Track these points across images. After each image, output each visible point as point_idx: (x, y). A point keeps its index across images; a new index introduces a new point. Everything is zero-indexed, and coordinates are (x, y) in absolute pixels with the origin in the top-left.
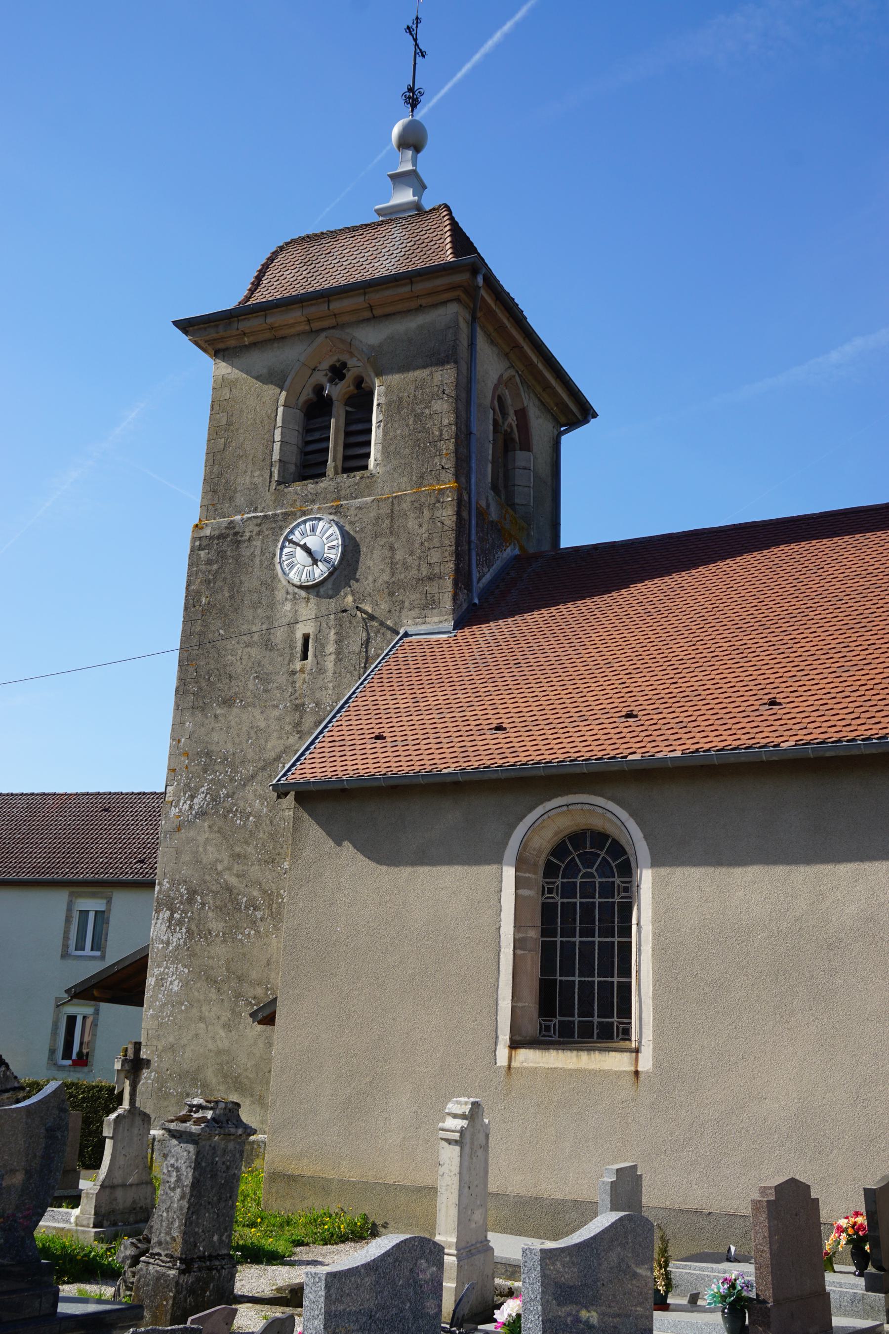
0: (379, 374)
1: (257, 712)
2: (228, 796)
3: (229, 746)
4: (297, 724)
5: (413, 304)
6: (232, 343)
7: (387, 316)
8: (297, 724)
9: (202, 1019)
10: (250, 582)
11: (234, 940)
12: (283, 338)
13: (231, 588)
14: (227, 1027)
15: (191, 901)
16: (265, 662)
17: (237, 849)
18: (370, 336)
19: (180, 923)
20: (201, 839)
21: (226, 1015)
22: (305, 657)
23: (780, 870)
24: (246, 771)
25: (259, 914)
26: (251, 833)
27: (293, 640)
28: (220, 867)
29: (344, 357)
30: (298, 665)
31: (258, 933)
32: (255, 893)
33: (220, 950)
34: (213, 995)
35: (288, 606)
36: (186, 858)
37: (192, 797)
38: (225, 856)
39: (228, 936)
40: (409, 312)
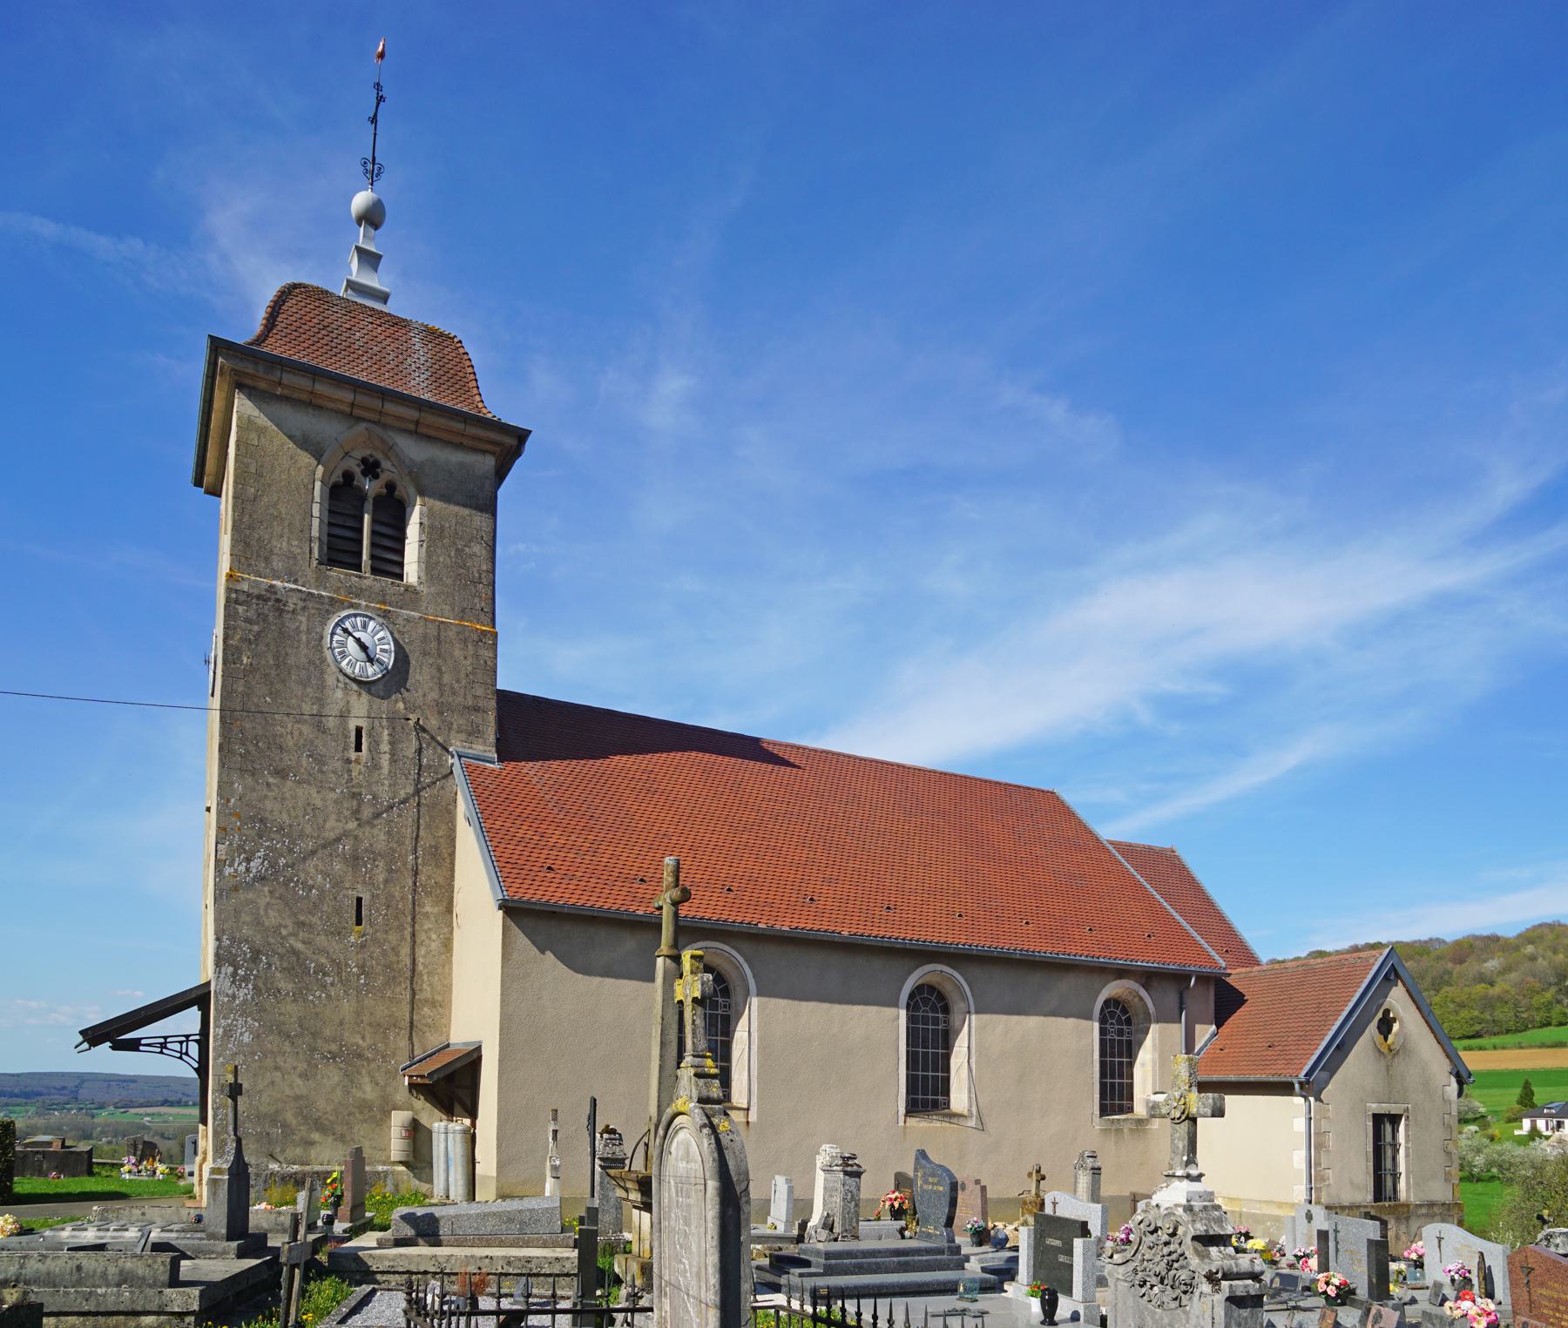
0: (422, 493)
1: (313, 791)
2: (287, 865)
3: (285, 816)
4: (356, 813)
5: (458, 439)
6: (262, 385)
8: (356, 813)
9: (277, 1068)
10: (299, 655)
12: (320, 407)
13: (276, 656)
14: (304, 1076)
15: (255, 958)
16: (318, 742)
17: (302, 918)
18: (414, 450)
19: (245, 979)
20: (262, 902)
21: (302, 1066)
22: (358, 748)
23: (826, 1006)
25: (329, 980)
27: (345, 728)
28: (284, 932)
29: (379, 456)
30: (353, 755)
31: (329, 997)
32: (323, 960)
33: (291, 1010)
34: (287, 1047)
35: (339, 694)
36: (245, 918)
37: (248, 860)
38: (289, 922)
39: (299, 996)
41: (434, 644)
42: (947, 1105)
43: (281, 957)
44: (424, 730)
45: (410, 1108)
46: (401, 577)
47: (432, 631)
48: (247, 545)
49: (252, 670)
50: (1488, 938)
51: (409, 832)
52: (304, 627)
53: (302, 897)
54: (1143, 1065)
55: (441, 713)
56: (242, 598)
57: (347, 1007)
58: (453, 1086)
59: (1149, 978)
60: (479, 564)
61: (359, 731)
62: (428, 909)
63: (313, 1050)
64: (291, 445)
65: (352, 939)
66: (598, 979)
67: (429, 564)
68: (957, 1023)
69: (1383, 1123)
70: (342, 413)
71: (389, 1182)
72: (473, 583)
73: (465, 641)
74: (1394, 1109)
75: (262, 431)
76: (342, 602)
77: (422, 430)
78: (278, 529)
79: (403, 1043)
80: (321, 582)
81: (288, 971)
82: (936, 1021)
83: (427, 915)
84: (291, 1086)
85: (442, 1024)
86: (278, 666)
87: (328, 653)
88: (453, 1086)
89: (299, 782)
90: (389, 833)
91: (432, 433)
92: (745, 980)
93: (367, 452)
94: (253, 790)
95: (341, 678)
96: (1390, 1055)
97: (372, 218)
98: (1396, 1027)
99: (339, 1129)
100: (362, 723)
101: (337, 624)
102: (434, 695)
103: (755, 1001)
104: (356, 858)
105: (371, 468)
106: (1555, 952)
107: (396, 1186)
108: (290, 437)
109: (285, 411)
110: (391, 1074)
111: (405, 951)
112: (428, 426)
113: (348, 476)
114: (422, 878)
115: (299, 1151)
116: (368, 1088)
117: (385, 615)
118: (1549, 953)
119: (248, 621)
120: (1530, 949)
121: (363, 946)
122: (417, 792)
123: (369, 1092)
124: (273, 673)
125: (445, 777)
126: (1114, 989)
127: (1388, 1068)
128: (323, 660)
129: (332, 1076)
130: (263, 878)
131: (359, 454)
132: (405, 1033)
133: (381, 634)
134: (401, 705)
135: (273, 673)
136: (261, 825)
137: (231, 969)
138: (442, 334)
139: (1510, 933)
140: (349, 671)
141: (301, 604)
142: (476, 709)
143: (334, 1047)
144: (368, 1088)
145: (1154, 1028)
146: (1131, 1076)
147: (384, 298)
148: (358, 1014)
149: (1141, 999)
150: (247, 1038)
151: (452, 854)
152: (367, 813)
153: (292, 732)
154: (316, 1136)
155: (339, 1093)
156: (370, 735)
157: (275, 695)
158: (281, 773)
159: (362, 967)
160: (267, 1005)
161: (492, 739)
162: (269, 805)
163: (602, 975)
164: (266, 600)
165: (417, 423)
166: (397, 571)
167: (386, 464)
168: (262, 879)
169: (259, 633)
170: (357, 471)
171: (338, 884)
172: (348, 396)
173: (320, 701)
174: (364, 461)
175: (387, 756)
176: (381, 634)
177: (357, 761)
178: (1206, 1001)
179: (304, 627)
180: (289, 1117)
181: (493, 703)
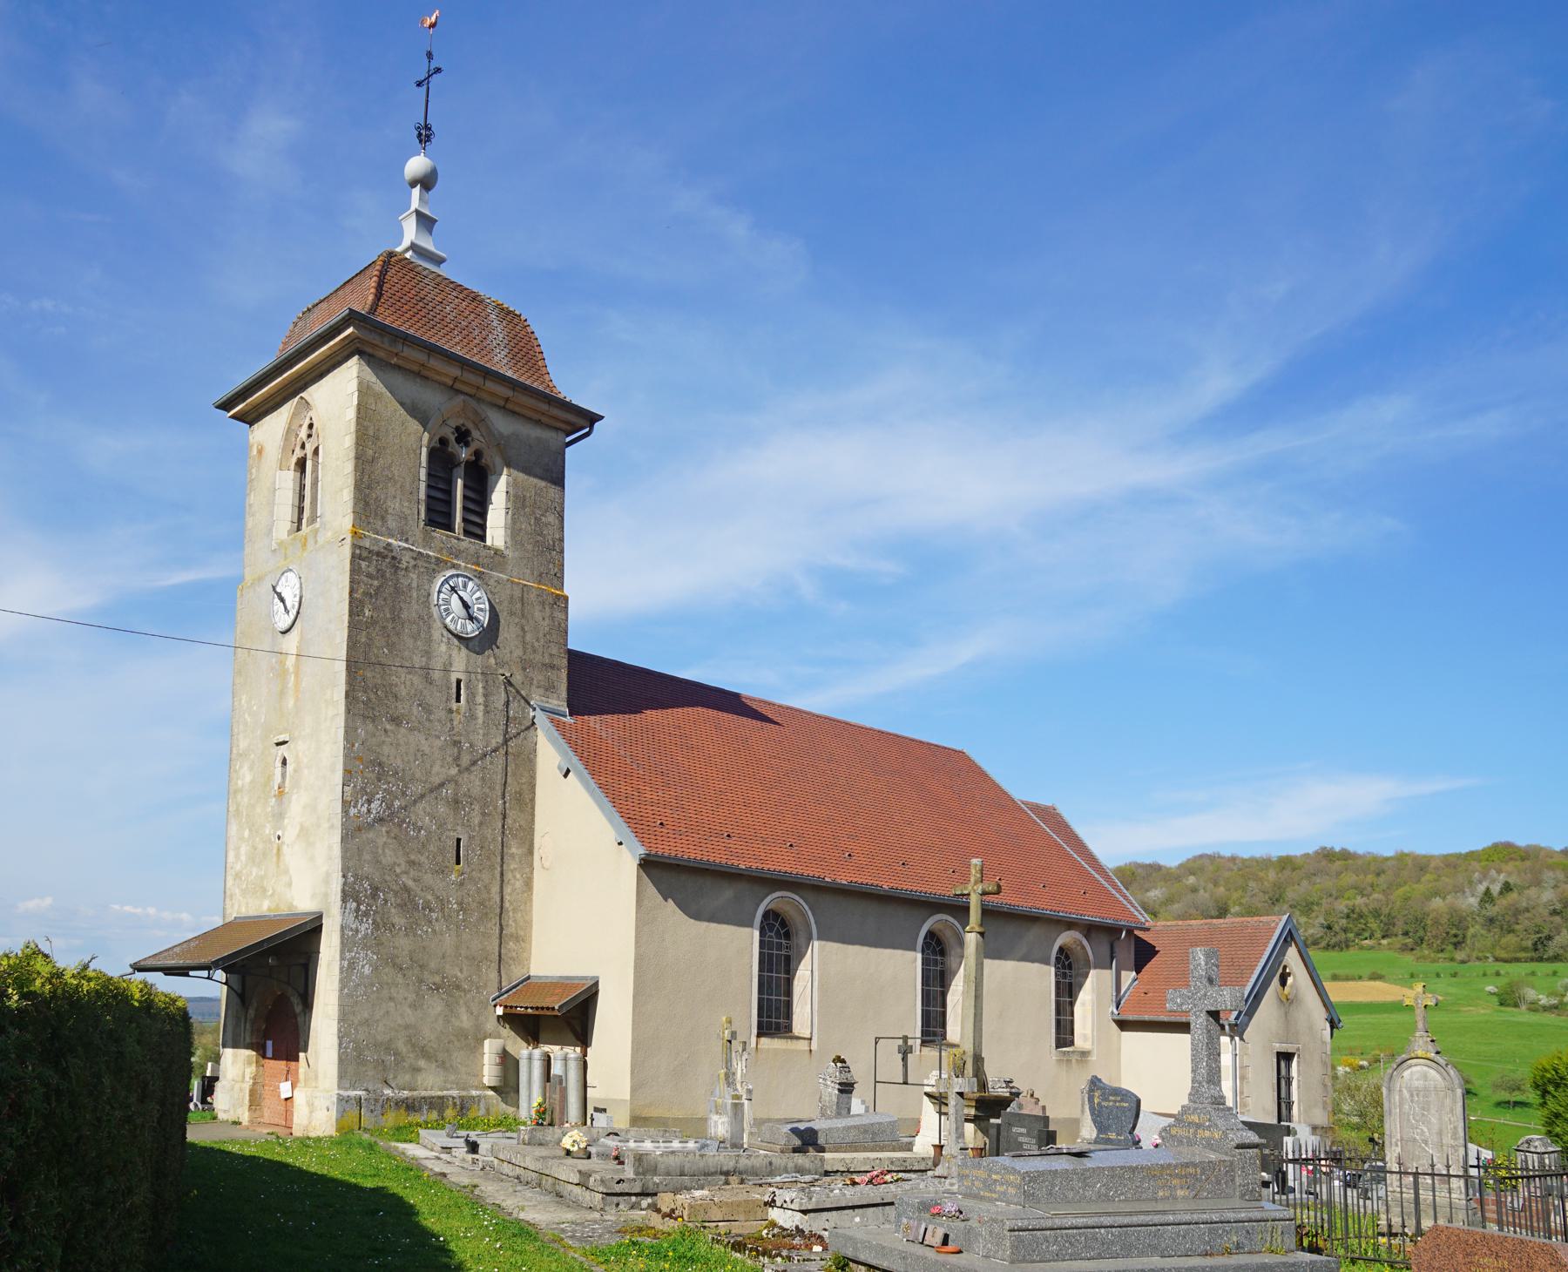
0: (509, 466)
1: (422, 738)
2: (401, 808)
3: (399, 762)
4: (457, 759)
5: (536, 417)
6: (381, 354)
7: (514, 413)
8: (457, 759)
9: (391, 999)
10: (410, 612)
11: (415, 935)
12: (427, 378)
13: (392, 611)
14: (413, 1006)
15: (374, 896)
16: (425, 692)
17: (413, 857)
18: (502, 424)
19: (366, 914)
20: (381, 841)
21: (412, 997)
22: (458, 700)
23: (866, 949)
24: (417, 789)
25: (434, 915)
26: (424, 846)
27: (448, 680)
28: (398, 870)
29: (470, 426)
30: (454, 706)
31: (434, 931)
32: (430, 897)
33: (404, 944)
34: (400, 979)
35: (443, 648)
36: (367, 857)
37: (369, 802)
38: (402, 861)
39: (410, 930)
40: (530, 419)
41: (519, 605)
42: (944, 1036)
43: (396, 893)
44: (511, 684)
45: (499, 1036)
46: (483, 538)
47: (517, 593)
48: (367, 504)
49: (373, 622)
50: (1150, 866)
51: (499, 778)
52: (414, 585)
53: (413, 838)
54: (1083, 1004)
55: (524, 669)
56: (365, 554)
57: (449, 940)
58: (572, 1018)
59: (1090, 929)
61: (459, 682)
62: (514, 850)
63: (421, 981)
64: (402, 411)
65: (453, 877)
66: (705, 924)
67: (513, 530)
68: (954, 966)
69: (1285, 1057)
70: (444, 384)
71: (482, 1105)
72: (544, 544)
73: (543, 603)
74: (1289, 1048)
75: (378, 396)
76: (446, 562)
77: (509, 406)
78: (392, 490)
79: (494, 975)
80: (427, 544)
81: (401, 906)
82: (779, 946)
84: (402, 1015)
85: (523, 960)
86: (393, 620)
87: (434, 610)
88: (572, 1018)
89: (411, 729)
90: (483, 779)
91: (517, 409)
92: (808, 925)
93: (460, 422)
96: (1288, 1003)
97: (426, 182)
98: (1290, 980)
99: (441, 1056)
100: (462, 676)
101: (446, 581)
102: (519, 652)
103: (816, 943)
105: (463, 436)
106: (1216, 884)
107: (488, 1110)
108: (402, 404)
110: (484, 1004)
111: (495, 889)
112: (464, 383)
113: (443, 441)
114: (509, 821)
115: (408, 1077)
116: (464, 1017)
117: (480, 576)
118: (1210, 886)
119: (369, 576)
120: (1192, 880)
121: (462, 884)
122: (506, 741)
123: (465, 1021)
124: (390, 626)
125: (528, 728)
126: (1066, 938)
127: (1286, 1014)
128: (430, 616)
129: (435, 1006)
130: (381, 820)
131: (453, 423)
132: (495, 965)
133: (478, 594)
134: (492, 661)
136: (380, 768)
137: (354, 905)
138: (509, 312)
139: (1172, 862)
140: (452, 627)
142: (552, 667)
143: (437, 979)
144: (464, 1017)
145: (1092, 972)
146: (1072, 1014)
147: (439, 261)
148: (457, 948)
149: (1083, 947)
150: (367, 970)
151: (533, 800)
152: (465, 760)
153: (405, 682)
154: (422, 1063)
155: (441, 1021)
156: (467, 688)
157: (391, 646)
158: (396, 720)
159: (460, 904)
160: (384, 939)
161: (564, 694)
162: (386, 750)
163: (709, 920)
164: (385, 557)
165: (507, 400)
166: (479, 532)
167: (475, 434)
168: (381, 820)
169: (378, 588)
170: (452, 438)
171: (442, 826)
172: (455, 371)
173: (428, 654)
174: (457, 429)
175: (481, 708)
176: (478, 594)
177: (458, 711)
178: (1127, 952)
179: (414, 585)
180: (401, 1045)
181: (565, 662)
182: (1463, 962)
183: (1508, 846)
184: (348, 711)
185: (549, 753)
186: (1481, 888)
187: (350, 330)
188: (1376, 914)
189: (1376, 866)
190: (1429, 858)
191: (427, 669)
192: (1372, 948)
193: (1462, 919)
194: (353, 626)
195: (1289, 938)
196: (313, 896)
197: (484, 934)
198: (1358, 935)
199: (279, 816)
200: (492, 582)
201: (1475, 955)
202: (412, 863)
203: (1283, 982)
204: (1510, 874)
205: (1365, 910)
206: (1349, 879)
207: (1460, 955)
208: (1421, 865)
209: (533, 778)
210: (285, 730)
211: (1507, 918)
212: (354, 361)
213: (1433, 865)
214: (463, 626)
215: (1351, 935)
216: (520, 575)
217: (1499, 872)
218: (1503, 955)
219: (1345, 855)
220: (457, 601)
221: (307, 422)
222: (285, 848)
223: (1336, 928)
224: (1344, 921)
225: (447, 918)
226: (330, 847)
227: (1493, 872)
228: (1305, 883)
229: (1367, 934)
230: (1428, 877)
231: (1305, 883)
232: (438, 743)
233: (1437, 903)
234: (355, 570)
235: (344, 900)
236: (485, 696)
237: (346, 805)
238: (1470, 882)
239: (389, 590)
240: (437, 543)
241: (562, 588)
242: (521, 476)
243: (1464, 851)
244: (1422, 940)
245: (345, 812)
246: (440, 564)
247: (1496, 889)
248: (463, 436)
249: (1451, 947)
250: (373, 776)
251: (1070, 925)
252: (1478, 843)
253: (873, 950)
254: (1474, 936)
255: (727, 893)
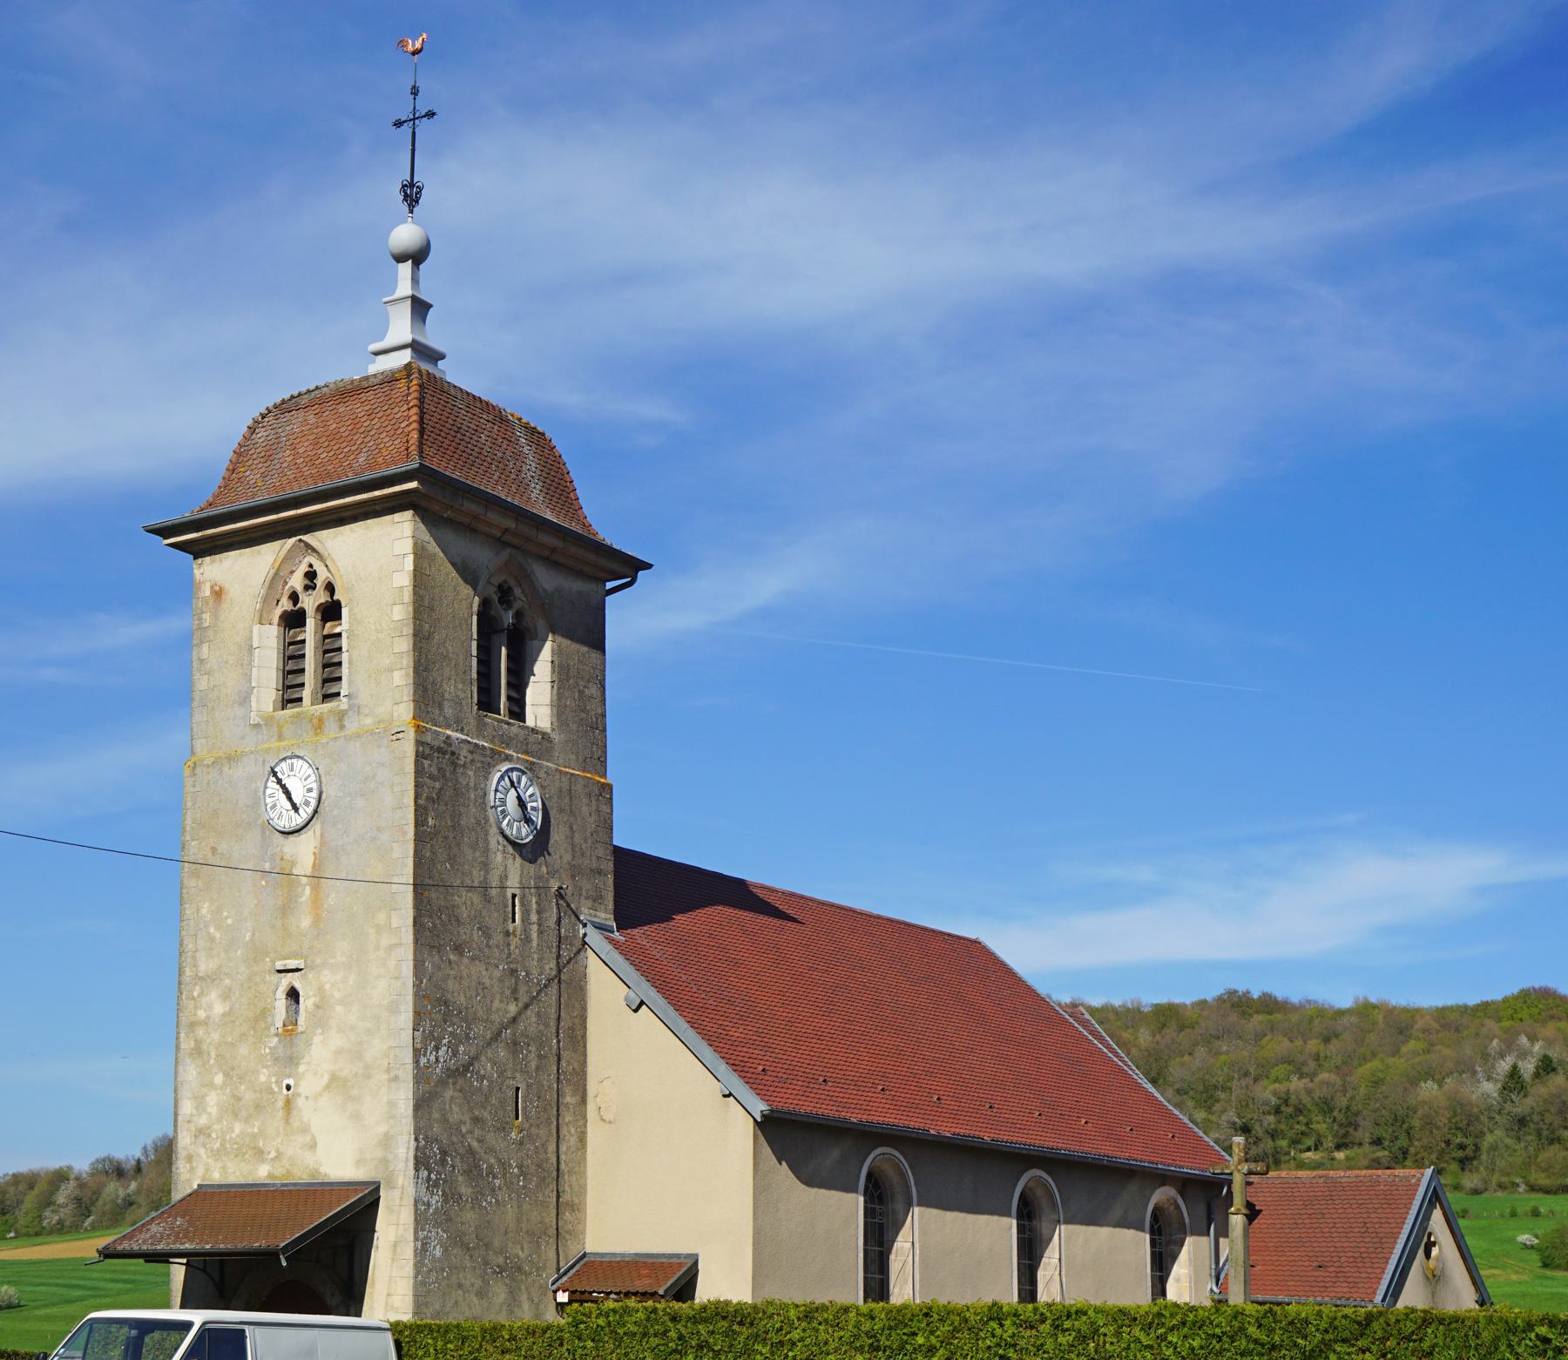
8: (515, 991)
9: (460, 1286)
12: (474, 531)
14: (481, 1294)
15: (443, 1162)
16: (484, 912)
18: (546, 579)
19: (436, 1185)
21: (478, 1282)
25: (497, 1182)
27: (505, 896)
29: (512, 583)
35: (499, 857)
37: (437, 1048)
38: (467, 1118)
39: (476, 1202)
41: (567, 800)
44: (562, 897)
47: (565, 785)
48: (425, 690)
49: (436, 832)
51: (554, 1016)
54: (1178, 1280)
55: (573, 877)
56: (427, 751)
60: (593, 706)
63: (486, 1263)
65: (513, 1135)
68: (1045, 1232)
73: (589, 795)
75: (432, 557)
76: (500, 753)
79: (552, 1254)
81: (467, 1172)
83: (567, 1106)
84: (470, 1307)
85: (578, 1234)
87: (491, 813)
89: (473, 959)
94: (439, 968)
95: (501, 839)
97: (417, 257)
98: (1435, 1251)
100: (517, 892)
101: (502, 778)
104: (515, 1043)
108: (454, 565)
109: (449, 535)
111: (552, 1147)
114: (563, 1064)
117: (531, 767)
121: (521, 1143)
124: (451, 835)
126: (1162, 1195)
131: (496, 581)
132: (552, 1241)
134: (544, 869)
135: (451, 835)
140: (508, 832)
141: (470, 757)
142: (600, 872)
143: (501, 1260)
144: (526, 1306)
145: (1189, 1240)
148: (518, 1220)
149: (1178, 1207)
150: (438, 1252)
151: (584, 1036)
153: (466, 902)
156: (522, 904)
157: (452, 859)
158: (458, 949)
159: (520, 1167)
160: (452, 1213)
161: (611, 906)
164: (444, 753)
165: (554, 550)
167: (517, 592)
170: (496, 598)
173: (485, 866)
182: (1476, 1192)
183: (1546, 994)
184: (416, 941)
185: (607, 986)
186: (1504, 1066)
187: (414, 485)
188: (1326, 1107)
189: (1322, 1024)
190: (1414, 1013)
191: (485, 887)
192: (1317, 1166)
193: (1472, 1119)
194: (419, 838)
195: (1434, 1197)
196: (360, 1162)
197: (542, 1203)
198: (1295, 1142)
199: (289, 1061)
200: (542, 774)
201: (1495, 1179)
202: (476, 1120)
203: (1428, 1255)
204: (1550, 1043)
205: (1306, 1100)
206: (1277, 1046)
207: (1470, 1180)
208: (1401, 1023)
209: (584, 1009)
210: (295, 955)
211: (1548, 1118)
212: (409, 514)
213: (1420, 1024)
214: (519, 829)
215: (1283, 1143)
216: (563, 763)
217: (1533, 1039)
218: (1543, 1180)
219: (1269, 1005)
220: (509, 798)
221: (303, 568)
222: (300, 1102)
223: (1258, 1130)
224: (1271, 1118)
225: (509, 1185)
226: (392, 1104)
227: (1524, 1040)
228: (1201, 1051)
229: (1310, 1142)
230: (1412, 1045)
231: (1201, 1051)
232: (497, 974)
233: (1429, 1089)
234: (419, 772)
235: (417, 1169)
236: (539, 912)
237: (417, 1053)
238: (1485, 1056)
239: (449, 793)
240: (489, 731)
241: (604, 776)
242: (566, 642)
243: (1473, 1001)
244: (1405, 1153)
245: (416, 1062)
246: (496, 757)
247: (1528, 1067)
248: (505, 594)
249: (1454, 1166)
250: (439, 1017)
251: (1163, 1178)
252: (1498, 990)
253: (971, 1218)
254: (1494, 1148)
255: (833, 1154)
